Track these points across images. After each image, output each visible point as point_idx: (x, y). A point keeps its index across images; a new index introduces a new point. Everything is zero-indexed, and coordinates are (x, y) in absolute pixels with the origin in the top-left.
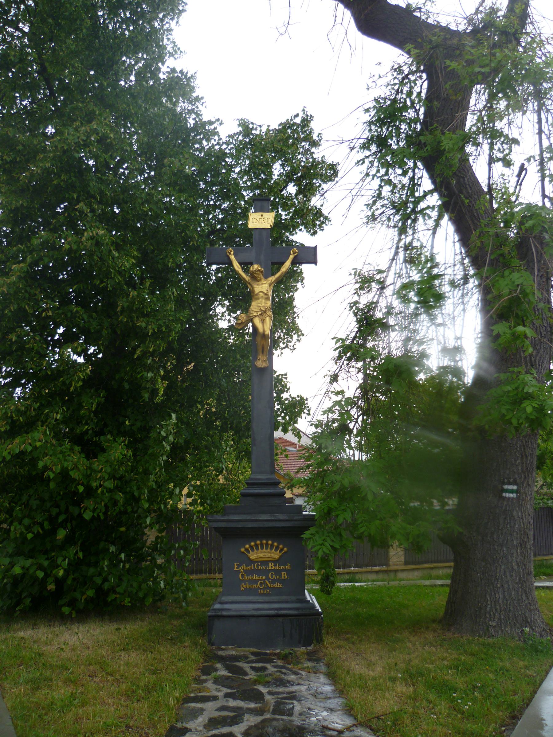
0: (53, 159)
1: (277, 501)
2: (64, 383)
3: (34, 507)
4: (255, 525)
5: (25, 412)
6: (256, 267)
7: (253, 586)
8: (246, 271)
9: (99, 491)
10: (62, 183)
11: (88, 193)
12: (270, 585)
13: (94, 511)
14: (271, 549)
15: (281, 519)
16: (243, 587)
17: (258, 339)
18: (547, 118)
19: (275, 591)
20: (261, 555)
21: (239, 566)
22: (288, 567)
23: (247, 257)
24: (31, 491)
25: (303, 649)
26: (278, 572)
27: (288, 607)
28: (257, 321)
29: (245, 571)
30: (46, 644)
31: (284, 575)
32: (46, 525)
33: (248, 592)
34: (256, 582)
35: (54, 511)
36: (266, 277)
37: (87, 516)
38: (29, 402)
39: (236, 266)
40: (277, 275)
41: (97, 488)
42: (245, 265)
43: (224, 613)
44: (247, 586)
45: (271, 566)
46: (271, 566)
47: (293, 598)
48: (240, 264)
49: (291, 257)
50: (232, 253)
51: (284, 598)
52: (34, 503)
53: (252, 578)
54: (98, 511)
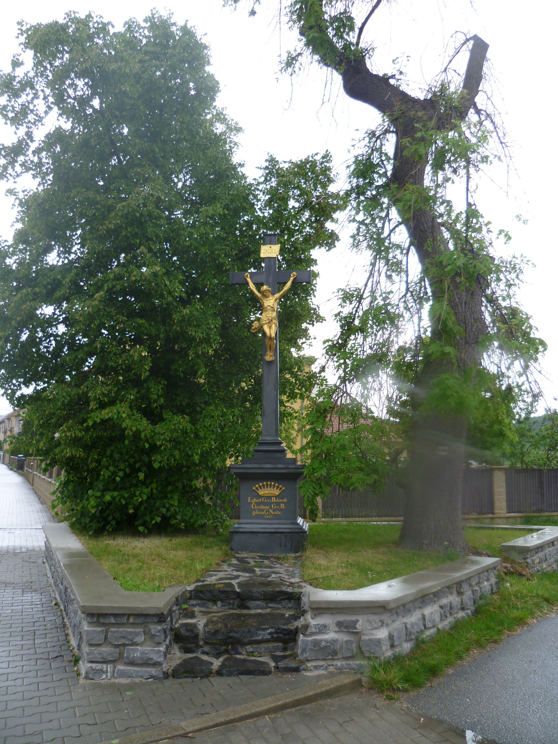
0: (122, 217)
1: (279, 455)
2: (135, 374)
3: (117, 459)
4: (262, 471)
5: (108, 394)
6: (265, 287)
7: (261, 513)
8: (259, 291)
9: (162, 448)
10: (128, 234)
11: (147, 237)
13: (160, 462)
14: (274, 488)
15: (280, 468)
16: (254, 513)
17: (267, 341)
19: (275, 517)
20: (266, 492)
21: (251, 499)
22: (285, 500)
23: (260, 279)
24: (113, 448)
25: (293, 555)
26: (278, 504)
27: (285, 527)
28: (266, 328)
29: (256, 503)
30: (124, 546)
31: (282, 506)
32: (127, 470)
33: (258, 517)
34: (263, 510)
35: (132, 461)
36: (273, 294)
37: (156, 465)
38: (110, 388)
39: (252, 286)
40: (281, 293)
41: (161, 446)
42: (258, 285)
43: (241, 530)
44: (257, 513)
45: (274, 499)
46: (274, 499)
47: (289, 522)
48: (254, 284)
49: (292, 279)
51: (282, 521)
52: (117, 456)
54: (163, 462)
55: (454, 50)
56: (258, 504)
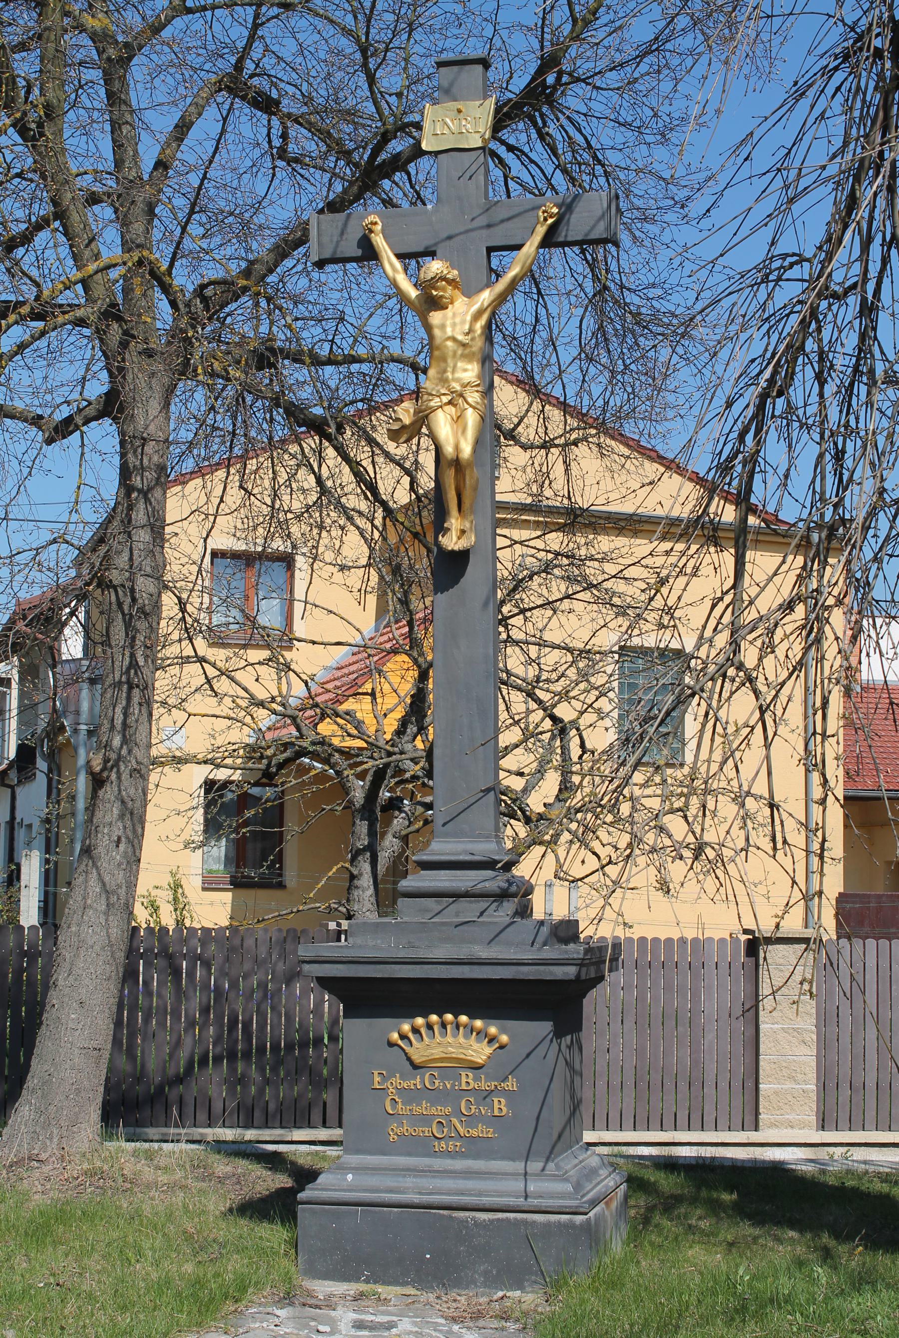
12: (461, 1131)
15: (504, 951)
16: (395, 1131)
18: (857, 422)
31: (500, 1105)
34: (425, 1120)
44: (406, 1128)
50: (379, 227)
53: (417, 1110)
55: (505, 904)
56: (410, 1096)
